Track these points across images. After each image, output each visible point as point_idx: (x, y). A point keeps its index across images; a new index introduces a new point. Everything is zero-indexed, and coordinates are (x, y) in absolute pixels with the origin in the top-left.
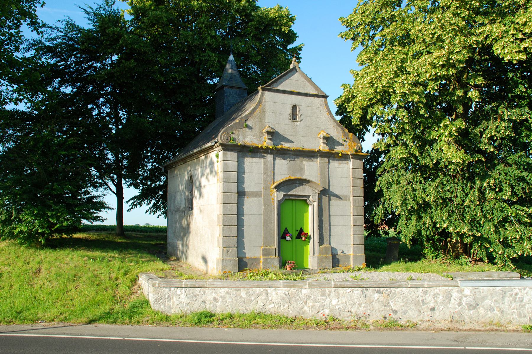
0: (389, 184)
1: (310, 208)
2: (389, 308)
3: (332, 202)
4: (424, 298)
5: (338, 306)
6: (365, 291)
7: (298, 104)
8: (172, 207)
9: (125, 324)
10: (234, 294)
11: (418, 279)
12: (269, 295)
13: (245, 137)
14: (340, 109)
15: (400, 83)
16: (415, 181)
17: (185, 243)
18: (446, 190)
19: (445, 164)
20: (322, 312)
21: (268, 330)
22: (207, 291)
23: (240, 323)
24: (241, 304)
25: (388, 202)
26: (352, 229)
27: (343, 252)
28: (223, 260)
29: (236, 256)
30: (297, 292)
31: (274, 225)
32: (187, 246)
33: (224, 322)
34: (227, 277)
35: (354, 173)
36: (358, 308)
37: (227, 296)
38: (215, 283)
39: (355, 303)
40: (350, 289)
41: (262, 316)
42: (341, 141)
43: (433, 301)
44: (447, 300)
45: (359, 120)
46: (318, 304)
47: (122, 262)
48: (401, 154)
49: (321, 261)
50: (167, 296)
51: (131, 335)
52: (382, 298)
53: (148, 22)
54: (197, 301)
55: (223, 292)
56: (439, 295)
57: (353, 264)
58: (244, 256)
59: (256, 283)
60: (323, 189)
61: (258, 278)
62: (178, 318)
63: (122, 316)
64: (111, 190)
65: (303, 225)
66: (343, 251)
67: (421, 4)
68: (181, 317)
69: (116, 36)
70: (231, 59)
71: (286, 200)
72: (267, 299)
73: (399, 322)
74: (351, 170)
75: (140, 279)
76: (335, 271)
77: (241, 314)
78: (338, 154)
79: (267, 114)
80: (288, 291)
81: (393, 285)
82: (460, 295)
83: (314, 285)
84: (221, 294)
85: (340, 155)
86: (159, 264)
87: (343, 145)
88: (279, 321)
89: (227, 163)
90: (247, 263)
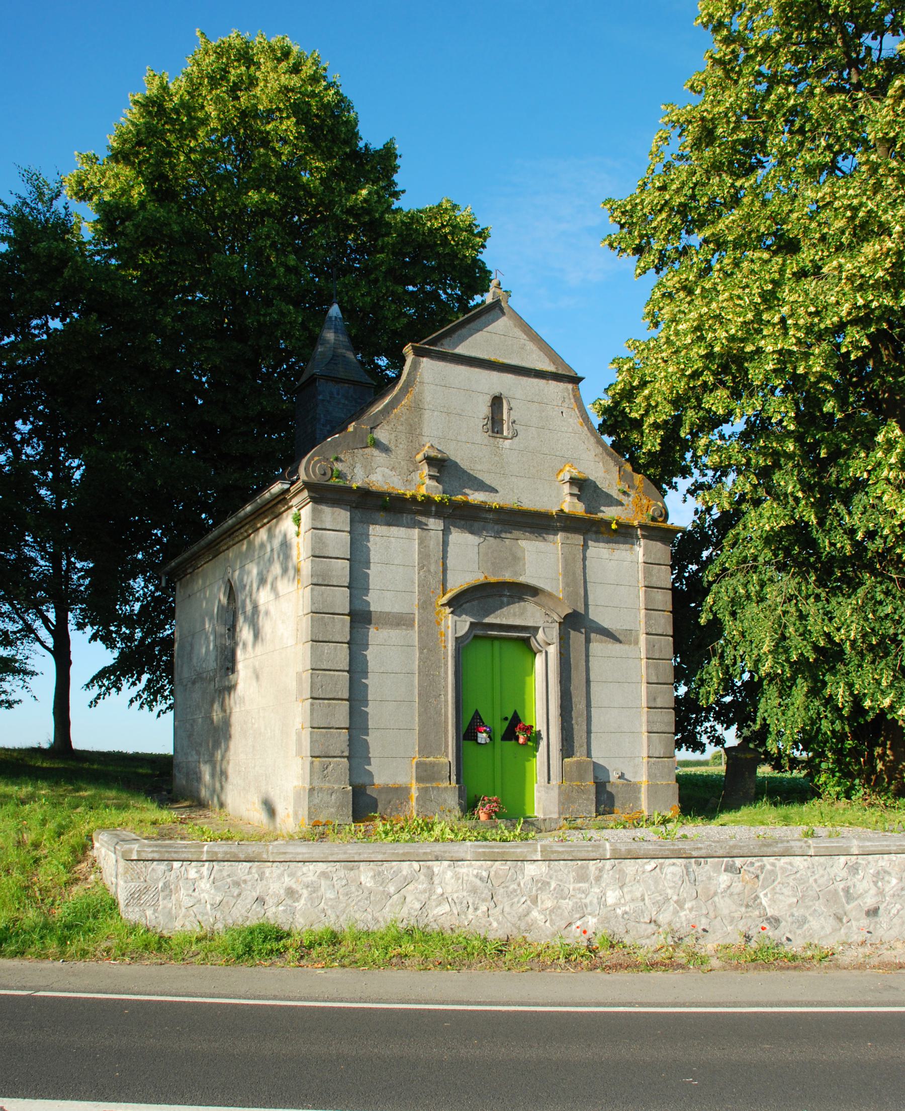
0: (735, 606)
1: (539, 660)
2: (757, 913)
3: (593, 646)
4: (850, 883)
5: (623, 908)
6: (694, 866)
7: (505, 393)
8: (186, 674)
9: (48, 958)
10: (340, 878)
11: (830, 836)
12: (436, 880)
13: (369, 472)
14: (611, 415)
15: (774, 325)
16: (804, 594)
17: (218, 769)
18: (882, 615)
19: (885, 542)
20: (579, 923)
21: (436, 972)
22: (267, 872)
23: (358, 956)
24: (361, 904)
25: (733, 652)
26: (644, 719)
27: (622, 777)
28: (312, 790)
30: (512, 871)
31: (446, 701)
32: (224, 774)
33: (314, 953)
34: (323, 836)
35: (647, 574)
36: (676, 913)
37: (323, 882)
38: (290, 849)
39: (667, 900)
40: (653, 863)
41: (417, 936)
42: (615, 494)
43: (873, 891)
45: (658, 441)
46: (567, 904)
47: (54, 805)
48: (772, 519)
49: (566, 799)
50: (161, 885)
51: (55, 985)
52: (740, 885)
53: (136, 232)
55: (310, 871)
56: (889, 874)
57: (649, 808)
58: (366, 780)
59: (401, 849)
60: (570, 611)
61: (405, 836)
62: (191, 943)
63: (41, 938)
64: (42, 644)
65: (523, 706)
66: (623, 774)
67: (811, 158)
68: (199, 940)
69: (54, 263)
70: (335, 315)
71: (476, 637)
72: (431, 891)
73: (783, 950)
74: (641, 566)
75: (97, 845)
77: (359, 932)
78: (608, 523)
79: (427, 415)
80: (488, 870)
81: (769, 850)
83: (556, 852)
84: (305, 879)
85: (614, 526)
86: (151, 812)
87: (621, 504)
88: (465, 948)
89: (322, 534)
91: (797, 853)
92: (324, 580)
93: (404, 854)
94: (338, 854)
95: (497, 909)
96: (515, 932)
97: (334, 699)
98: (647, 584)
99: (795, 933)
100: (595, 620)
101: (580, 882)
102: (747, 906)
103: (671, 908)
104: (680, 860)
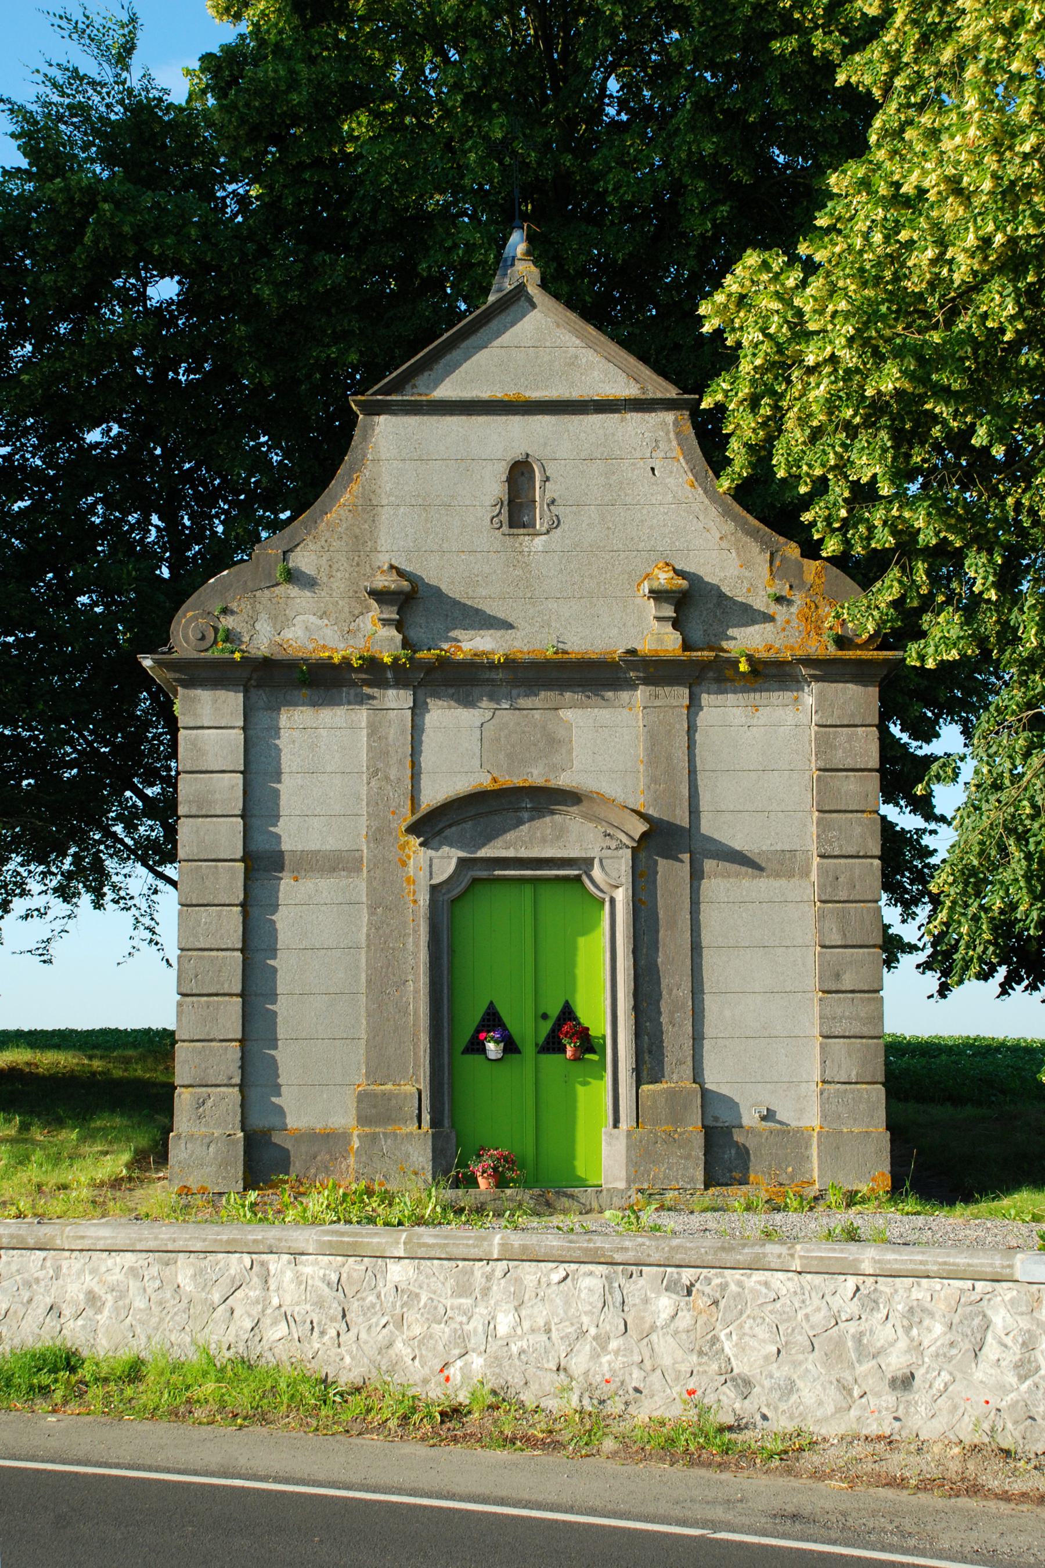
2: (715, 1367)
4: (864, 1326)
5: (519, 1344)
7: (535, 451)
10: (153, 1278)
12: (273, 1284)
13: (280, 621)
20: (459, 1363)
22: (65, 1264)
24: (177, 1318)
29: (238, 1125)
35: (823, 745)
43: (903, 1344)
44: (966, 1345)
46: (442, 1331)
54: (34, 1304)
56: (931, 1314)
65: (574, 991)
71: (475, 881)
72: (266, 1303)
76: (720, 1202)
79: (385, 514)
81: (728, 1258)
82: (1024, 1323)
85: (743, 667)
90: (288, 1151)
91: (773, 1266)
92: (200, 808)
93: (229, 1242)
94: (147, 1239)
95: (350, 1333)
96: (374, 1373)
97: (217, 995)
98: (821, 765)
99: (776, 1409)
100: (716, 836)
101: (460, 1296)
102: (701, 1353)
103: (588, 1347)
104: (601, 1268)
